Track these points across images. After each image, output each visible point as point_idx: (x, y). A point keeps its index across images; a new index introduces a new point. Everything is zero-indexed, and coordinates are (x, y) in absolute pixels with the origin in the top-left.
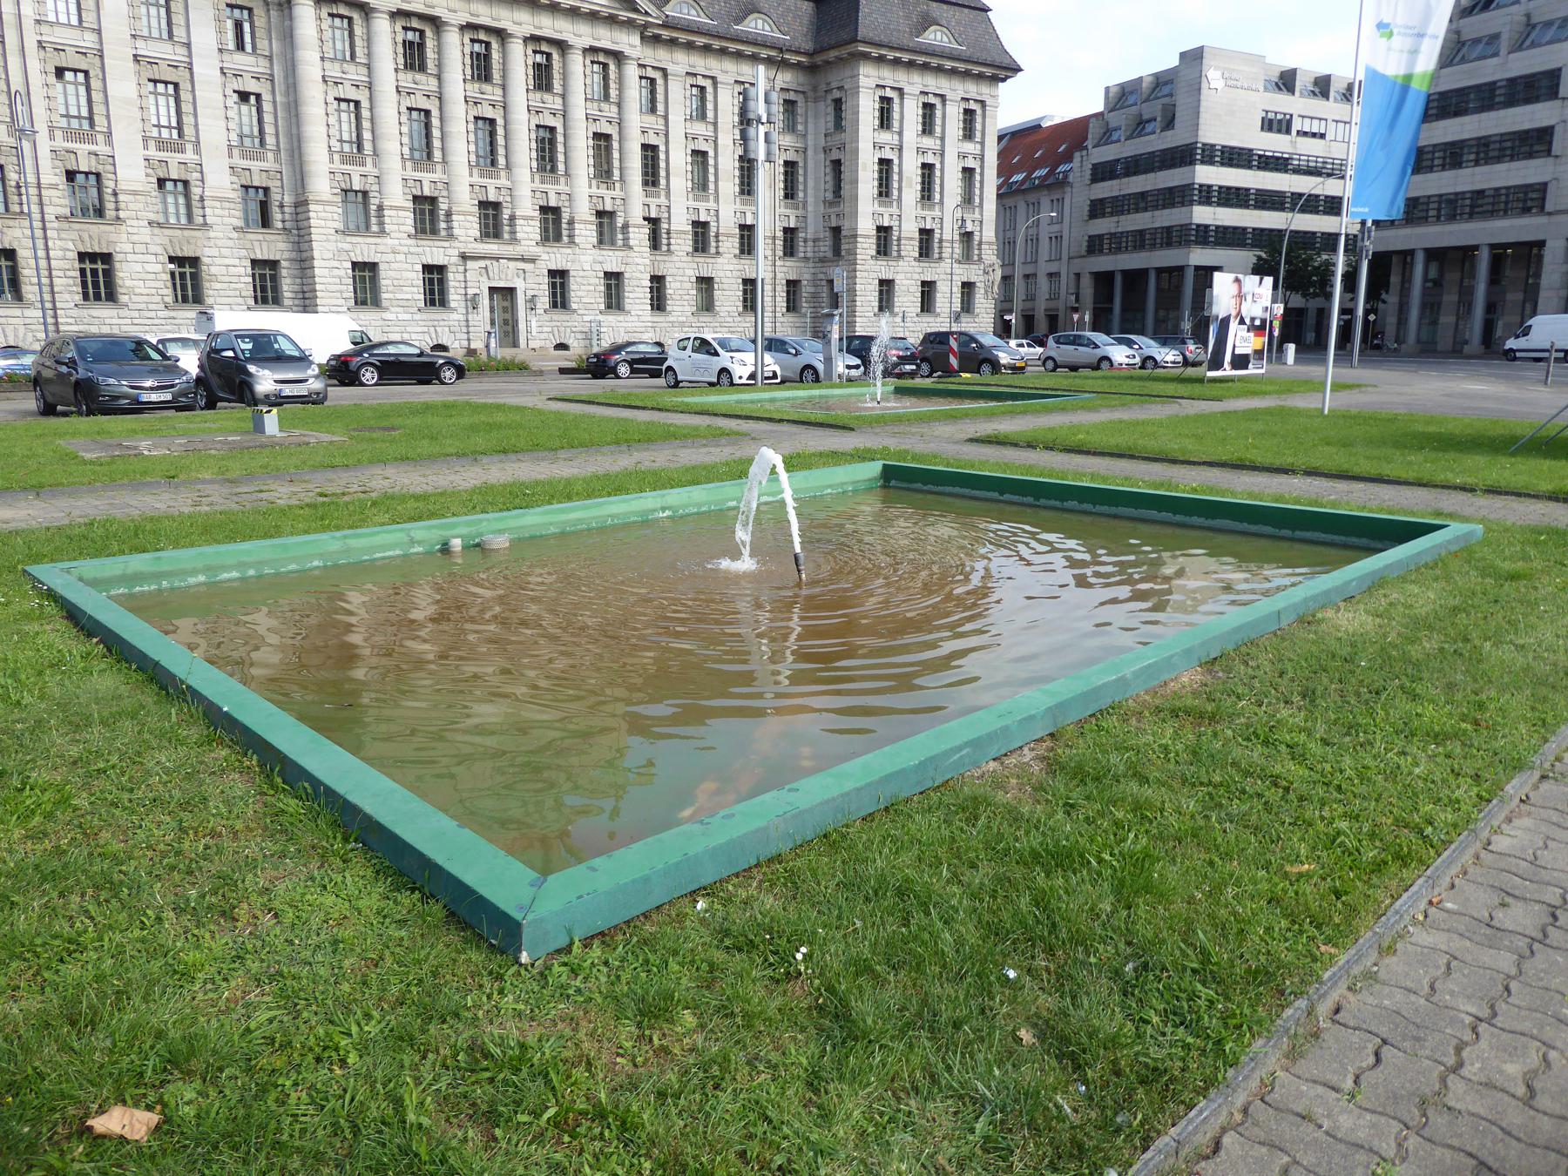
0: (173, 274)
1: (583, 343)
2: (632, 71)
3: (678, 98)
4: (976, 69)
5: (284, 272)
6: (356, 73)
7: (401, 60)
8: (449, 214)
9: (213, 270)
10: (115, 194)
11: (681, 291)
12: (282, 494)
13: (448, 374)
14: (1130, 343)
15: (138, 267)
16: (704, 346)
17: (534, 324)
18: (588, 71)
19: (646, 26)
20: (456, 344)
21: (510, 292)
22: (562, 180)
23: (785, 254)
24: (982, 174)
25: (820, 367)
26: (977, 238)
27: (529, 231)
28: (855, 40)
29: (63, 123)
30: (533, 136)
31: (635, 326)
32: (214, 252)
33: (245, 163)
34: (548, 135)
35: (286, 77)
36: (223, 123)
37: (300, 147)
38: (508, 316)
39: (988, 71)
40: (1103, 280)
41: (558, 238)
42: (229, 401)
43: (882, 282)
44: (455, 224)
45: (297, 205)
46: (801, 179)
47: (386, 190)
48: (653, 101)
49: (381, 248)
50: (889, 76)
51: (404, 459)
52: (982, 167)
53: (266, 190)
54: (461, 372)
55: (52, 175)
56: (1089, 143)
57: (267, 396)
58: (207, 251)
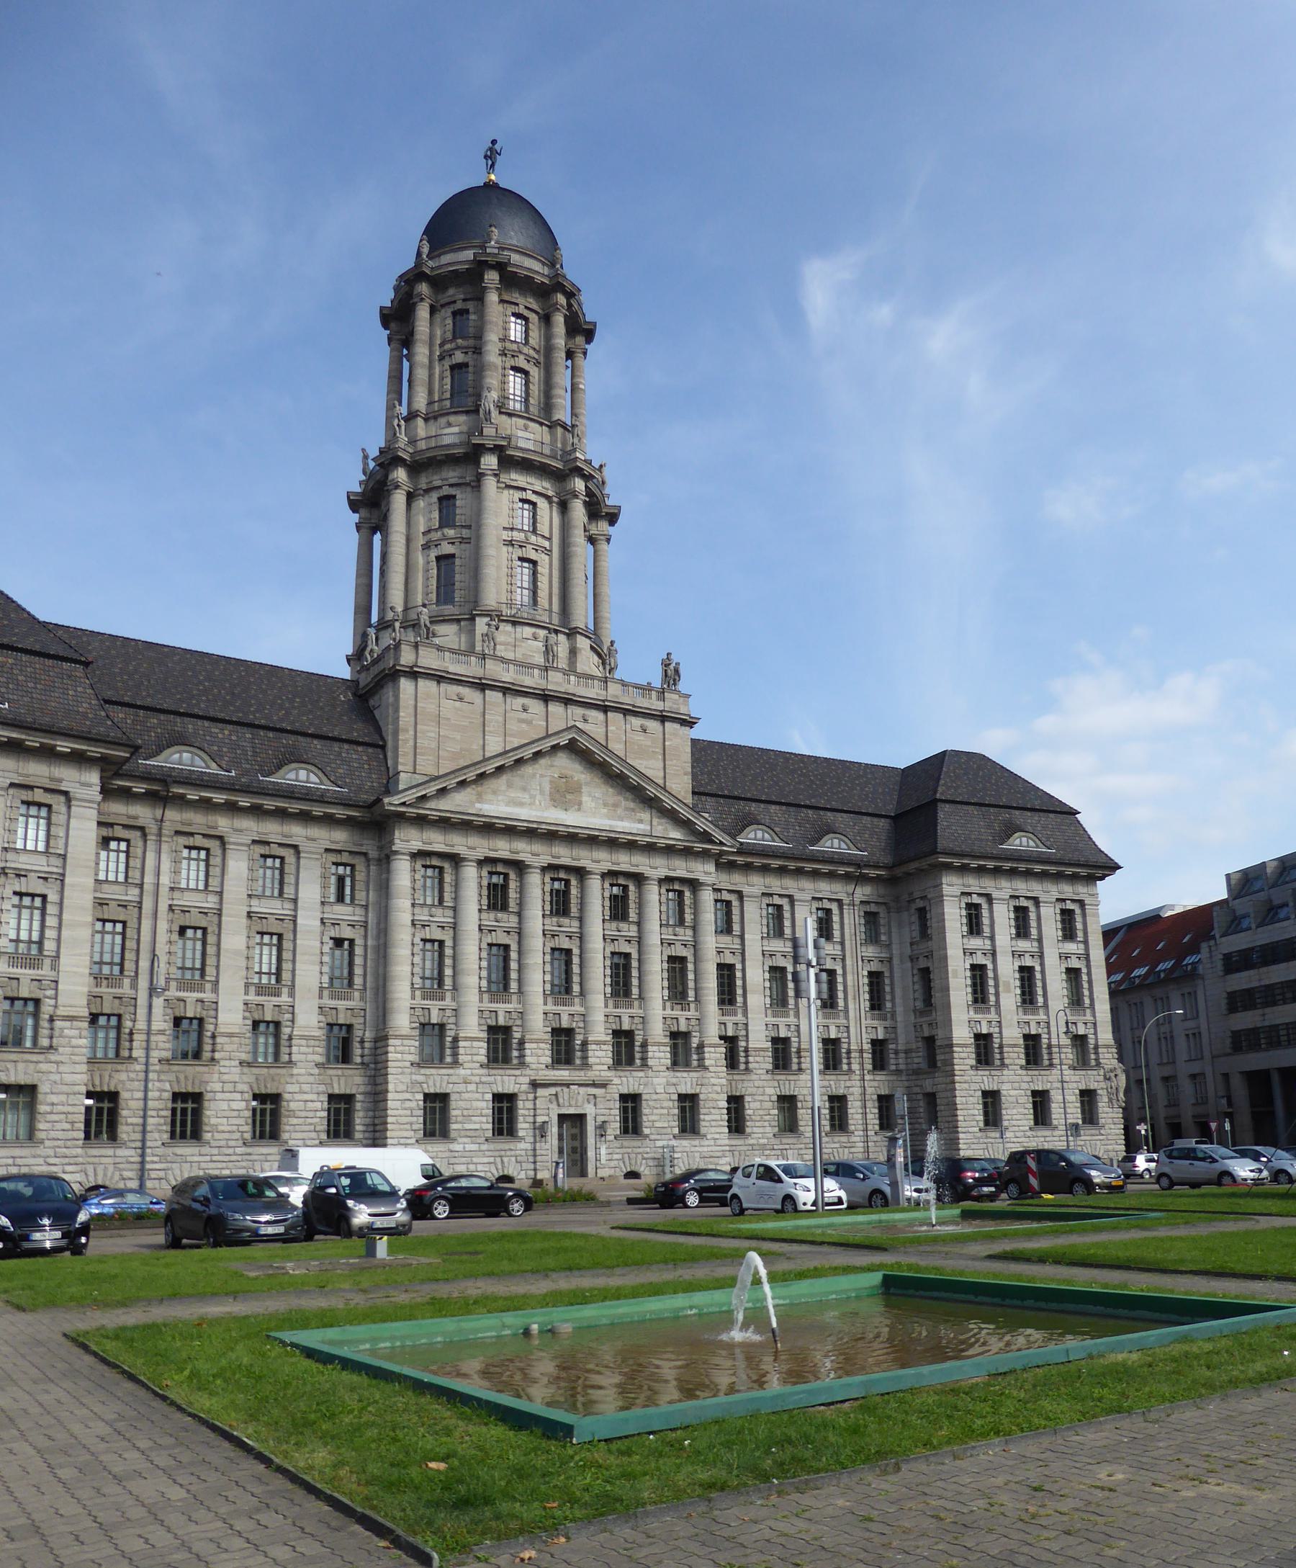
0: (254, 1110)
1: (654, 1171)
2: (707, 897)
3: (754, 918)
4: (1069, 871)
5: (358, 1106)
6: (443, 916)
7: (485, 901)
8: (522, 1042)
9: (293, 1105)
10: (214, 1037)
11: (761, 1112)
12: (402, 1298)
13: (517, 1207)
14: (1256, 1157)
15: (224, 1106)
16: (768, 1174)
17: (603, 1151)
18: (664, 899)
19: (722, 853)
20: (522, 1175)
21: (580, 1119)
22: (636, 1003)
23: (875, 1068)
24: (1089, 974)
25: (887, 1190)
26: (1092, 1041)
27: (601, 1056)
28: (934, 852)
29: (179, 974)
30: (608, 963)
31: (712, 1151)
32: (294, 1088)
33: (333, 1003)
34: (622, 961)
35: (378, 923)
36: (317, 968)
37: (385, 986)
38: (577, 1144)
39: (1083, 872)
40: (1258, 1080)
41: (630, 1061)
42: (326, 1234)
43: (986, 1094)
44: (528, 1052)
45: (376, 1040)
46: (888, 989)
47: (463, 1021)
48: (729, 922)
49: (453, 1079)
50: (974, 884)
51: (490, 1275)
52: (1088, 966)
53: (349, 1027)
54: (529, 1204)
55: (161, 1022)
56: (1216, 932)
57: (361, 1228)
58: (290, 1088)
